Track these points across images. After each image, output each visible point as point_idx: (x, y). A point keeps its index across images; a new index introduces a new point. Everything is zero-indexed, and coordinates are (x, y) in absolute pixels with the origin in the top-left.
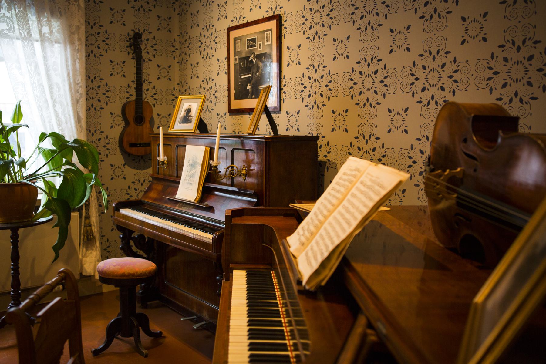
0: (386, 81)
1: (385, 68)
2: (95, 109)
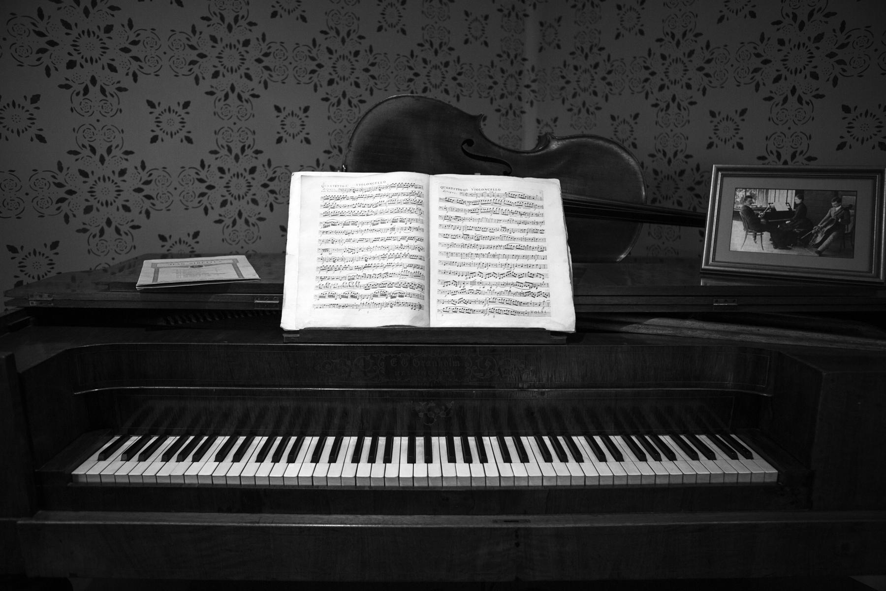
0: (610, 78)
1: (609, 60)
2: (118, 231)
